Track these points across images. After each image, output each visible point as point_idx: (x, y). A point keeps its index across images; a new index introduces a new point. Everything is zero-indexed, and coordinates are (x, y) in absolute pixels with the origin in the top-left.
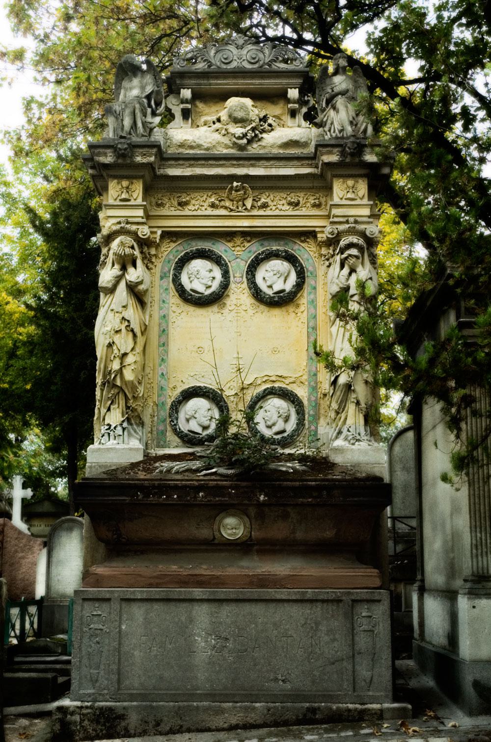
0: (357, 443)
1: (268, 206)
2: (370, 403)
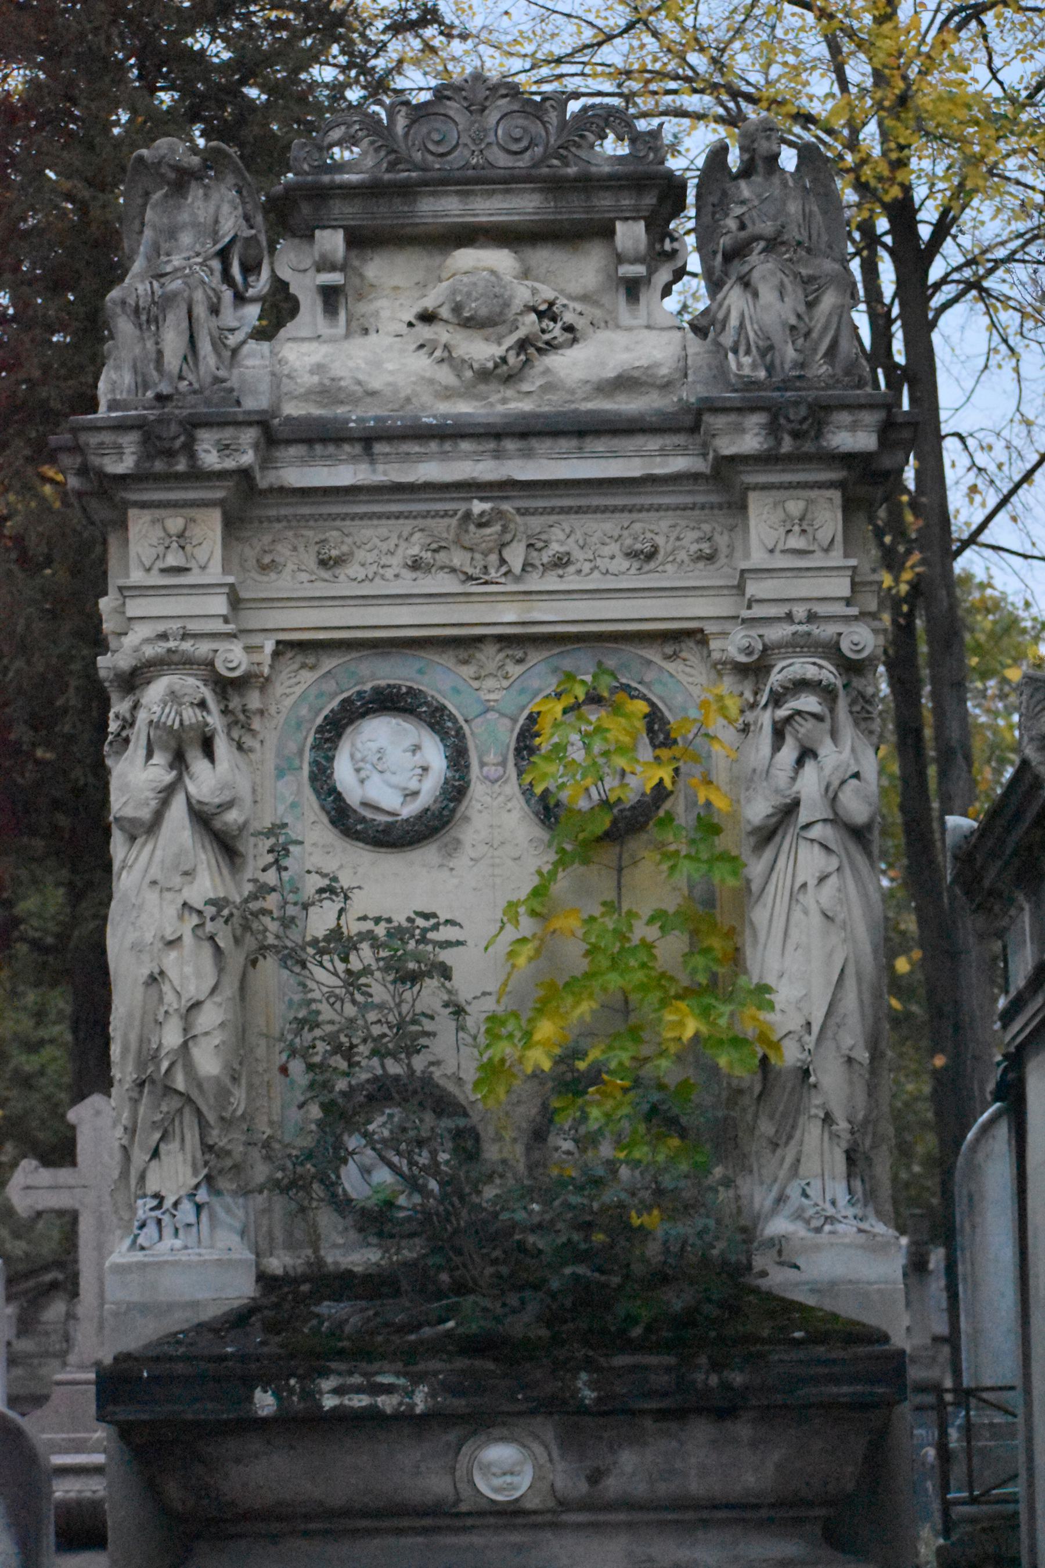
0: (827, 1228)
1: (568, 563)
2: (860, 1116)
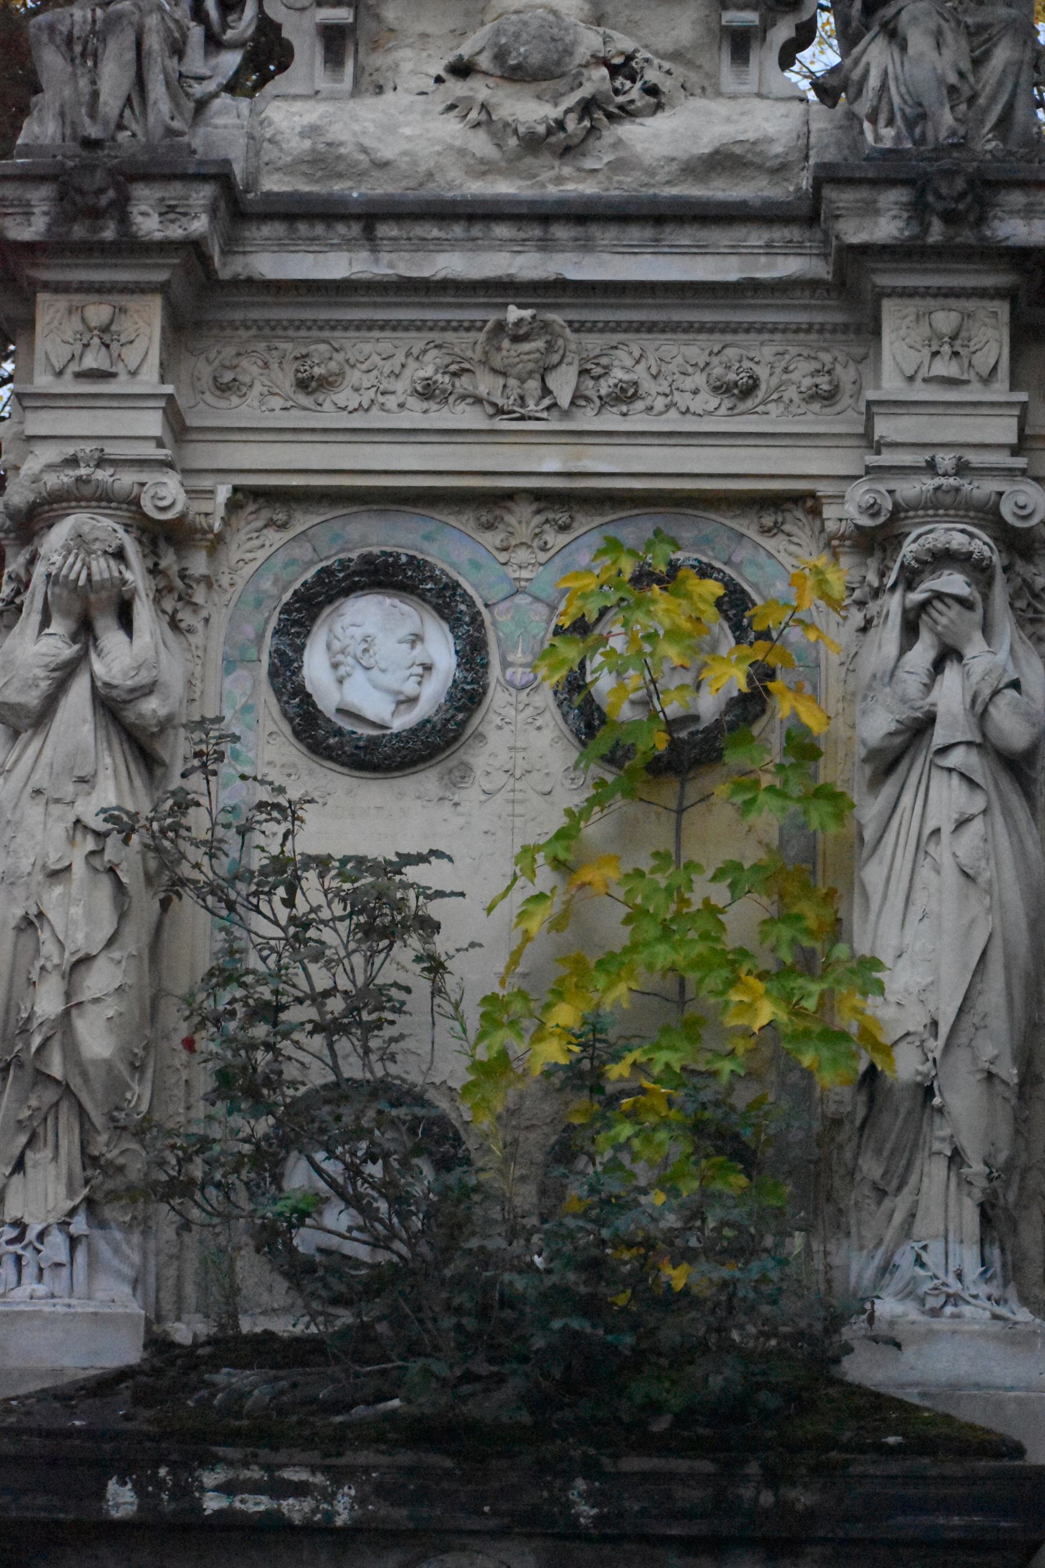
1: (635, 397)
2: (1002, 1157)
